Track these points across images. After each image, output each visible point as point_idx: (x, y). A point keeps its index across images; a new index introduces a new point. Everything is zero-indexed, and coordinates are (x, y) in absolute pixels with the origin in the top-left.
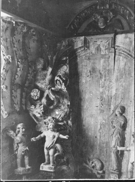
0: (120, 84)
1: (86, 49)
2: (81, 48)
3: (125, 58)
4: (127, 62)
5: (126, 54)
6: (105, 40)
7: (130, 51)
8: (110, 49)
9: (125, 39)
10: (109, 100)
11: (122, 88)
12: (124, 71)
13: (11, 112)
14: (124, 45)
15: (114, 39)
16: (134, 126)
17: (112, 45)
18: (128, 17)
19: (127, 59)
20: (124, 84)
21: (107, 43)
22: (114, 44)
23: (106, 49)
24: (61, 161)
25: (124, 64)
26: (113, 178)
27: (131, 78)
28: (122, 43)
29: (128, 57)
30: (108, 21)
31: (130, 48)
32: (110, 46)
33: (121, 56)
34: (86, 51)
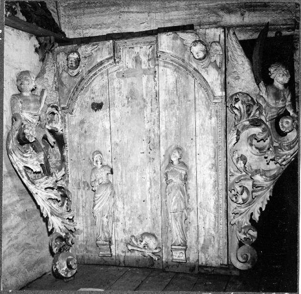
1: (117, 60)
2: (108, 59)
3: (175, 70)
9: (174, 41)
11: (175, 120)
21: (151, 50)
23: (149, 60)
34: (117, 64)
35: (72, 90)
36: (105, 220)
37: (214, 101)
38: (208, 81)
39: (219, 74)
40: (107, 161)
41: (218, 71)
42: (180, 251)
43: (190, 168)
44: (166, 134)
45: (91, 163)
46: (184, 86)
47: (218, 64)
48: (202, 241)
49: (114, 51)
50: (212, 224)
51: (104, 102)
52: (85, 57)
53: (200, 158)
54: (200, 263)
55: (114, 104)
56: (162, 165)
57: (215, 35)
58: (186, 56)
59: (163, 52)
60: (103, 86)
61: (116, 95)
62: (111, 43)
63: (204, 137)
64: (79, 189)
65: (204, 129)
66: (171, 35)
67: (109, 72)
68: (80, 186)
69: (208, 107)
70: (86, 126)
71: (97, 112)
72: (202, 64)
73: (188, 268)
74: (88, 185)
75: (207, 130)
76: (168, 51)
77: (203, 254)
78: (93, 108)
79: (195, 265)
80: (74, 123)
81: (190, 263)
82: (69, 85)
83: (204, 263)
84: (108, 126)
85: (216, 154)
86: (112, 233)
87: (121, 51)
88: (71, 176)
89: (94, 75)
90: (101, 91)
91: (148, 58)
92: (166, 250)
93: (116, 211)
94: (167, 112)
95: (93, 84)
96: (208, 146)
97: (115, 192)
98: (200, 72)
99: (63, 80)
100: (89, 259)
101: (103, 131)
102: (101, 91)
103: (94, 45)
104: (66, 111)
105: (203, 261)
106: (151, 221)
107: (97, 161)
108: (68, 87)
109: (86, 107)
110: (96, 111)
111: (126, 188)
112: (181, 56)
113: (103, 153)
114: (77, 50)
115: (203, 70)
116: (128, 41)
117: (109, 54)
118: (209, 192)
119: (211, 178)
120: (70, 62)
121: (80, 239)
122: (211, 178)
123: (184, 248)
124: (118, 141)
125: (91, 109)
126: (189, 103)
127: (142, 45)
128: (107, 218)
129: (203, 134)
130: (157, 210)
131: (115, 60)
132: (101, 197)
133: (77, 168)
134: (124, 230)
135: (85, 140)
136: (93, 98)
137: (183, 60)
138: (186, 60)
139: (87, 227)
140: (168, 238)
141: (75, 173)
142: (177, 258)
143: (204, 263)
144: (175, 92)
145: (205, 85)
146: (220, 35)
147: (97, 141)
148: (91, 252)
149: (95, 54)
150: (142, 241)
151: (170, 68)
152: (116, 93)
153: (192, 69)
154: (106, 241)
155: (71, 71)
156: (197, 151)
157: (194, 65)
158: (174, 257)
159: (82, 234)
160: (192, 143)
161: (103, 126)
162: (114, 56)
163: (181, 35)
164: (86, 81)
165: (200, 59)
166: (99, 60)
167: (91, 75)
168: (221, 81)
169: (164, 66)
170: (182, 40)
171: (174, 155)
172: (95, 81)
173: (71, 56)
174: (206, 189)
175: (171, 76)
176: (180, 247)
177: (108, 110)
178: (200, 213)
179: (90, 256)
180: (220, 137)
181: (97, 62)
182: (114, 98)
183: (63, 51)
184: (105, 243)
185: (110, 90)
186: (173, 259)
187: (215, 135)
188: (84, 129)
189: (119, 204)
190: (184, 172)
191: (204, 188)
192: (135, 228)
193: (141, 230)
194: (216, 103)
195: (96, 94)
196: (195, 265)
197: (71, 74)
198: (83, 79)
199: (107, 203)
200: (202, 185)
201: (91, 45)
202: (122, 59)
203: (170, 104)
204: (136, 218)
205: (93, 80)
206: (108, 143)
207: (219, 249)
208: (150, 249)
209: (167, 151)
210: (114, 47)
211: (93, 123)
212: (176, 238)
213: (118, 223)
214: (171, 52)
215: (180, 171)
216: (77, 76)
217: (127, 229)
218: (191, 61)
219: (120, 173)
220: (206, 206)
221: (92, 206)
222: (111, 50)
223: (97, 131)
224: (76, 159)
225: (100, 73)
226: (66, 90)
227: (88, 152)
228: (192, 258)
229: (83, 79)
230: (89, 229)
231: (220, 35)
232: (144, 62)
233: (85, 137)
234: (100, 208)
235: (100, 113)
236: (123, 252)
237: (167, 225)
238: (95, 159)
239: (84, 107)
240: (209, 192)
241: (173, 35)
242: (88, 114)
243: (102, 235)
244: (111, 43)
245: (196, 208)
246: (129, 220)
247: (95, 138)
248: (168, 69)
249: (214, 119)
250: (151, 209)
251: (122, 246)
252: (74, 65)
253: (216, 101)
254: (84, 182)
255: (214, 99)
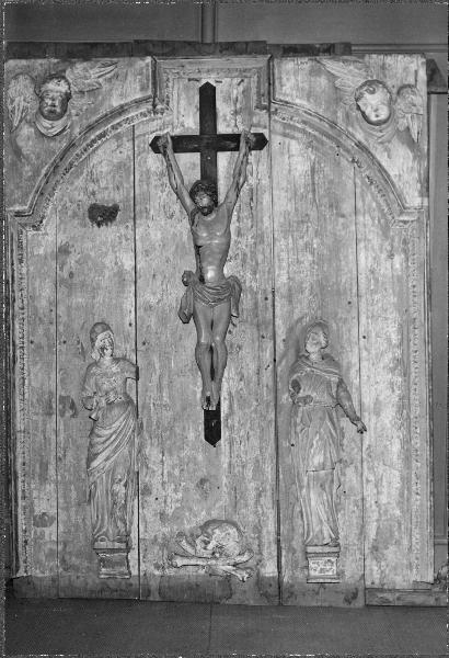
0: (301, 242)
1: (159, 107)
2: (138, 102)
3: (309, 145)
4: (255, 243)
5: (316, 133)
6: (232, 78)
8: (251, 114)
9: (313, 79)
10: (256, 304)
11: (310, 258)
13: (53, 592)
15: (270, 80)
16: (448, 347)
17: (259, 95)
21: (241, 88)
22: (270, 94)
23: (236, 113)
24: (43, 534)
25: (307, 167)
29: (322, 143)
32: (254, 104)
34: (159, 115)
35: (44, 172)
36: (120, 489)
37: (401, 218)
38: (392, 174)
39: (415, 158)
40: (125, 348)
41: (412, 151)
42: (327, 558)
43: (344, 368)
44: (290, 290)
45: (83, 353)
46: (331, 182)
47: (415, 136)
48: (372, 532)
49: (154, 84)
50: (395, 493)
51: (121, 206)
52: (82, 92)
53: (368, 346)
54: (368, 583)
55: (147, 211)
56: (280, 362)
57: (406, 69)
58: (339, 114)
59: (287, 102)
60: (120, 166)
61: (153, 191)
62: (147, 65)
63: (376, 297)
64: (50, 414)
65: (377, 280)
66: (305, 63)
67: (137, 133)
68: (51, 407)
69: (385, 231)
70: (72, 261)
71: (103, 228)
72: (380, 134)
73: (343, 596)
74: (73, 406)
75: (383, 283)
76: (298, 101)
77: (375, 562)
78: (92, 218)
79: (356, 589)
80: (41, 252)
81: (347, 584)
82: (38, 158)
83: (377, 582)
84: (128, 264)
85: (405, 337)
86: (131, 523)
87: (170, 84)
88: (30, 384)
89: (101, 136)
90: (114, 177)
91: (233, 108)
92: (290, 555)
93: (145, 470)
94: (290, 241)
95: (95, 160)
96: (386, 319)
97: (142, 423)
98: (373, 152)
99: (21, 143)
100: (71, 586)
101: (115, 275)
102: (114, 177)
103: (105, 66)
104: (24, 220)
105: (374, 575)
106: (229, 494)
107: (103, 349)
108: (34, 161)
109: (75, 215)
110: (99, 225)
111: (171, 413)
112: (328, 115)
113: (113, 328)
114: (65, 71)
115: (379, 147)
116: (190, 63)
117: (143, 89)
118: (387, 421)
119: (393, 391)
120: (50, 102)
121: (47, 538)
122: (393, 391)
123: (336, 550)
124: (153, 300)
125: (88, 220)
126: (341, 220)
127: (222, 74)
128: (125, 486)
129: (373, 292)
130: (243, 467)
131: (154, 106)
132: (114, 437)
133: (49, 364)
134: (161, 514)
135: (69, 295)
136: (93, 193)
137: (333, 125)
138: (340, 122)
139: (67, 509)
140: (293, 530)
141: (40, 374)
142: (317, 574)
143: (377, 582)
144: (310, 196)
145: (383, 181)
146: (416, 72)
147: (99, 299)
148: (77, 569)
149: (106, 87)
150: (207, 543)
151: (297, 139)
152: (152, 187)
153: (350, 144)
154: (120, 541)
155: (47, 123)
156: (362, 329)
157: (360, 136)
158: (312, 573)
159: (55, 525)
160: (349, 312)
161: (116, 264)
162: (155, 96)
163: (331, 65)
164: (78, 151)
165: (378, 123)
166: (116, 103)
167: (93, 137)
168: (420, 174)
169: (285, 135)
170: (332, 77)
171: (313, 339)
172: (100, 152)
173: (51, 85)
174: (383, 415)
175: (300, 158)
176: (327, 549)
177: (130, 224)
178: (369, 469)
179: (74, 578)
180: (416, 299)
181: (111, 106)
182: (147, 198)
183: (26, 72)
184: (117, 545)
185: (137, 177)
186: (308, 577)
187: (401, 296)
188: (66, 268)
189: (153, 453)
190: (335, 379)
191: (378, 414)
192: (190, 510)
193: (204, 513)
194: (405, 222)
195: (103, 185)
196: (356, 589)
197: (43, 131)
198: (72, 145)
199: (126, 451)
200: (372, 406)
201: (99, 65)
202: (171, 105)
203: (298, 223)
204: (192, 486)
205: (94, 151)
206: (129, 304)
207: (410, 548)
208: (227, 556)
209: (291, 330)
210: (154, 72)
211: (92, 254)
212: (317, 529)
213: (147, 498)
214: (305, 103)
215: (327, 376)
216: (58, 138)
217: (170, 511)
218: (353, 126)
219: (155, 378)
220: (383, 453)
221: (84, 457)
222: (148, 80)
223: (101, 273)
224: (44, 342)
225: (113, 133)
226: (27, 168)
227: (76, 326)
228: (351, 570)
229: (72, 145)
230: (73, 513)
231: (416, 72)
232: (225, 116)
233: (70, 287)
234: (108, 463)
235: (109, 233)
236: (157, 567)
237: (292, 500)
238: (98, 344)
239: (70, 213)
240: (387, 421)
241: (310, 63)
242: (79, 231)
243: (109, 528)
244: (147, 65)
245: (359, 458)
246: (176, 491)
247: (95, 290)
248: (293, 142)
249: (398, 259)
250: (230, 465)
251: (155, 554)
252: (58, 110)
253: (406, 218)
254: (63, 399)
255: (401, 213)
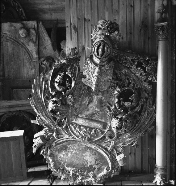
5: (13, 40)
7: (16, 38)
12: (13, 55)
14: (10, 32)
18: (18, 9)
19: (13, 44)
20: (14, 66)
26: (159, 185)
27: (20, 61)
28: (8, 30)
30: (2, 12)
31: (16, 36)
33: (8, 42)
